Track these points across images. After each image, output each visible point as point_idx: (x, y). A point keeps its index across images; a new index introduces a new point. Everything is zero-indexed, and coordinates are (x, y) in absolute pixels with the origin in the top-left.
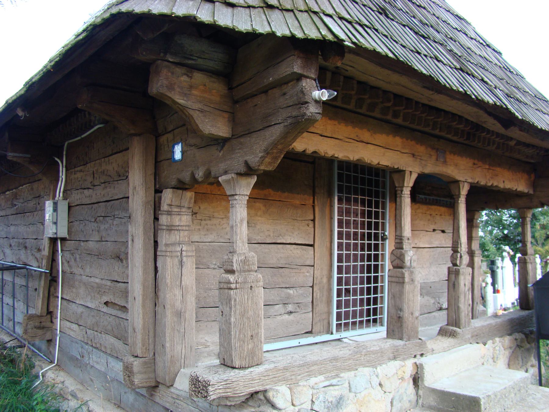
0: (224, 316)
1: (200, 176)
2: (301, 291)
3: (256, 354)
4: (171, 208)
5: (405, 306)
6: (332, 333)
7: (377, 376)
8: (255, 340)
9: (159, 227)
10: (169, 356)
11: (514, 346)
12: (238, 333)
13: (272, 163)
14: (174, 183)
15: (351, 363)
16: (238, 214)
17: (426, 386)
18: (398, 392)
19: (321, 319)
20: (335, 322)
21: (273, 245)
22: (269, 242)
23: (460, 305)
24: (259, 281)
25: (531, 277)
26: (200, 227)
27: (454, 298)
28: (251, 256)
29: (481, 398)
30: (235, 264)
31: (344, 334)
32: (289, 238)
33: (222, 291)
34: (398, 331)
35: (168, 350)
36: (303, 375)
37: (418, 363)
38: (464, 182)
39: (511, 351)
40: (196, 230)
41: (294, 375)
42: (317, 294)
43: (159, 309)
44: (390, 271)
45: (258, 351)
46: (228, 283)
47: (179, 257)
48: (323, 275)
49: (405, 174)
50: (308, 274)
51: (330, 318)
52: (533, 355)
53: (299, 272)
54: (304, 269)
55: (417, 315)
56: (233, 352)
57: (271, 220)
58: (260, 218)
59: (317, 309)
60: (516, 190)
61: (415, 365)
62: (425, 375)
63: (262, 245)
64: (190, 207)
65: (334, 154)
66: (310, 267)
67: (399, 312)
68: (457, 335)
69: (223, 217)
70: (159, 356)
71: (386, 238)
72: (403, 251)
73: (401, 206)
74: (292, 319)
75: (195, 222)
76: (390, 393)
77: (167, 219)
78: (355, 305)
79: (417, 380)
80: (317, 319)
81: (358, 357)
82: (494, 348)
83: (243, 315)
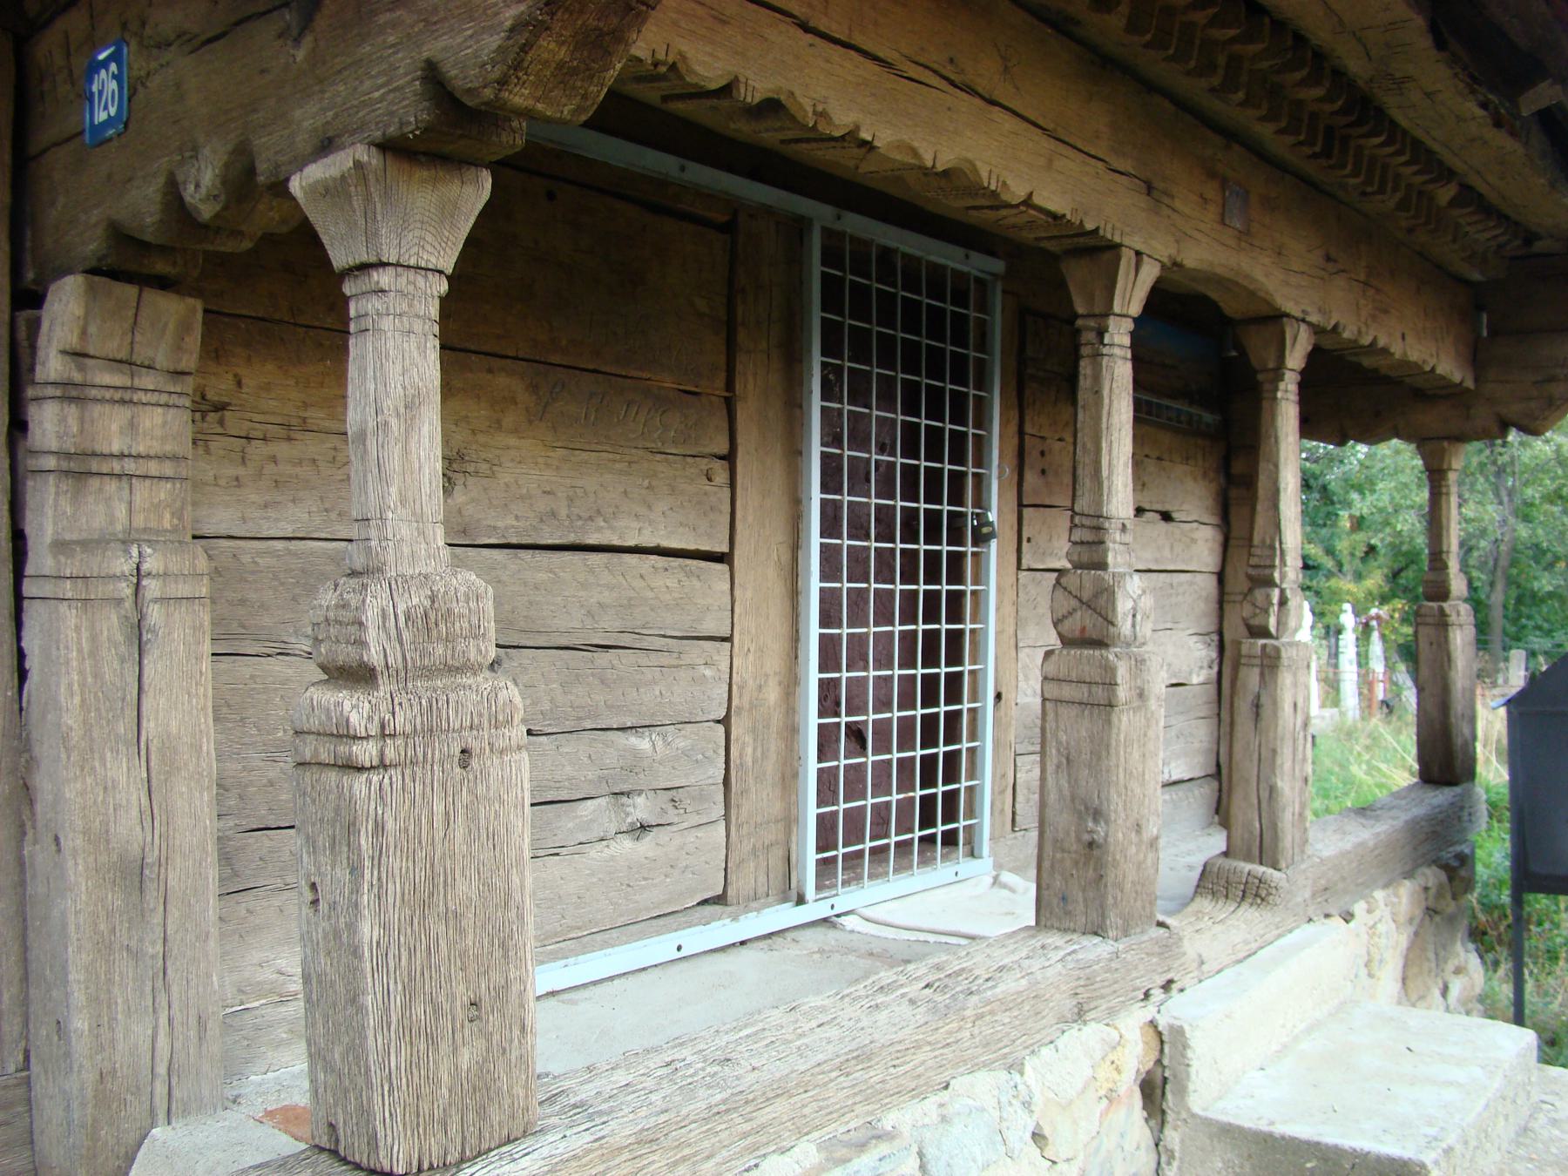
0: (323, 906)
1: (203, 191)
2: (682, 740)
3: (499, 1091)
4: (81, 369)
5: (1115, 797)
6: (801, 900)
7: (1027, 1105)
8: (494, 1020)
9: (32, 463)
10: (90, 1077)
11: (1418, 913)
12: (397, 1000)
13: (574, 72)
14: (92, 245)
15: (923, 1062)
16: (394, 371)
17: (1194, 1116)
18: (1097, 1150)
19: (759, 845)
20: (812, 856)
21: (567, 556)
22: (550, 542)
23: (1279, 784)
24: (509, 722)
25: (1460, 674)
26: (241, 471)
27: (1256, 756)
28: (463, 589)
29: (1430, 1166)
30: (372, 635)
31: (847, 898)
32: (636, 525)
33: (308, 776)
34: (1085, 900)
35: (81, 1047)
36: (725, 1153)
37: (1162, 1024)
38: (1297, 319)
39: (1411, 930)
40: (222, 482)
41: (684, 1159)
42: (743, 749)
43: (38, 853)
44: (1054, 658)
45: (509, 1073)
46: (340, 736)
47: (129, 604)
48: (767, 675)
49: (1118, 258)
50: (708, 672)
51: (794, 838)
52: (1459, 935)
53: (675, 662)
54: (696, 651)
55: (1155, 831)
56: (377, 1099)
57: (561, 452)
58: (512, 441)
59: (744, 811)
60: (1433, 370)
61: (1151, 1030)
62: (1193, 1070)
63: (522, 553)
64: (182, 366)
65: (857, 128)
66: (717, 644)
67: (1090, 824)
68: (1269, 894)
70: (46, 1072)
71: (991, 535)
72: (1107, 576)
73: (1098, 393)
74: (650, 854)
75: (217, 445)
76: (1068, 1160)
77: (63, 420)
78: (882, 787)
79: (1159, 1092)
80: (743, 848)
81: (950, 1033)
82: (1373, 927)
83: (421, 903)
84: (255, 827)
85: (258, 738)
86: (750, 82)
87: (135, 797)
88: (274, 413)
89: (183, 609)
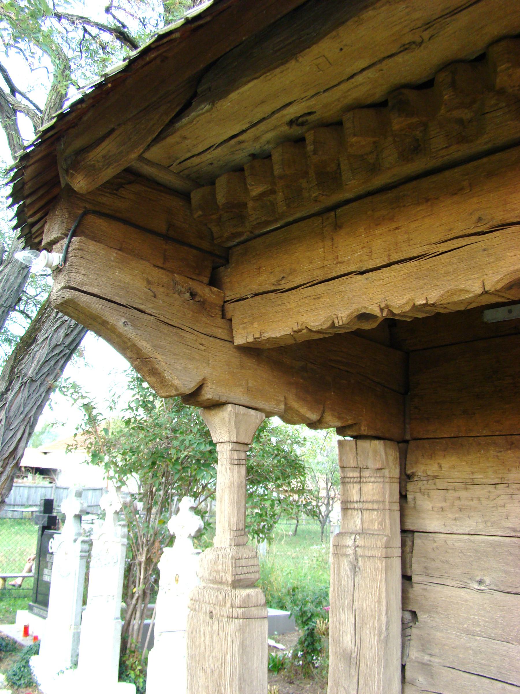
26: (444, 504)
40: (436, 509)
69: (496, 481)
84: (448, 665)
85: (455, 625)
86: (339, 316)
87: (349, 630)
88: (458, 478)
89: (371, 561)
